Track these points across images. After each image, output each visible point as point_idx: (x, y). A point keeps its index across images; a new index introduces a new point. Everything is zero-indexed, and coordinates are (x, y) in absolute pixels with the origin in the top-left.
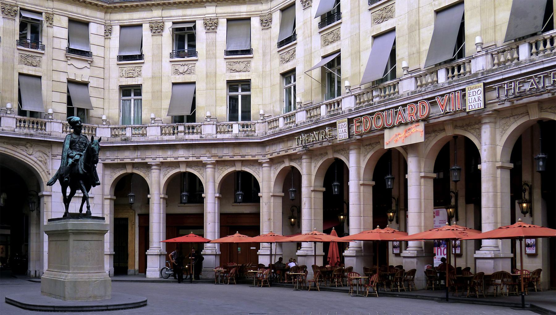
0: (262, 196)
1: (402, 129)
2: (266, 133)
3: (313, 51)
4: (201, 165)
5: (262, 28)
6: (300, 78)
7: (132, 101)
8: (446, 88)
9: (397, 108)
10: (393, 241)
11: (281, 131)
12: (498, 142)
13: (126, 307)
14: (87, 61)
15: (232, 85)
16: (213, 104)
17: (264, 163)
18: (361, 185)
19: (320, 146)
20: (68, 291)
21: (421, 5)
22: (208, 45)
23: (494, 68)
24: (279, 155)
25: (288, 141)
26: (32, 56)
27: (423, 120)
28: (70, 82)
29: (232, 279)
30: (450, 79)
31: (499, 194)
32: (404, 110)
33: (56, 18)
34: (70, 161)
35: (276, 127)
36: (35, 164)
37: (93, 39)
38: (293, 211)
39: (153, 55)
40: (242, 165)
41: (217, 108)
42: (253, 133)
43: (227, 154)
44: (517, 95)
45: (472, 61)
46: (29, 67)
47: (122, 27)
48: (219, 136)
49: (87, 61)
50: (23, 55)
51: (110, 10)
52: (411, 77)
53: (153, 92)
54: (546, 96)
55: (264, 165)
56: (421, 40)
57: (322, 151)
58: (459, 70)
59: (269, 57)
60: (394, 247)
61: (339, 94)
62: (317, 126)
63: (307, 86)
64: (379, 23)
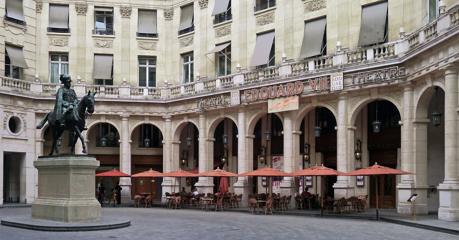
1: (282, 100)
2: (169, 97)
3: (208, 40)
4: (119, 118)
5: (165, 19)
7: (60, 64)
9: (279, 85)
10: (262, 176)
11: (182, 96)
12: (349, 113)
13: (110, 227)
14: (22, 29)
15: (142, 59)
16: (127, 73)
17: (167, 119)
20: (70, 214)
21: (295, 16)
22: (123, 27)
24: (180, 113)
25: (188, 103)
27: (297, 95)
28: (8, 45)
29: (178, 205)
30: (317, 69)
31: (349, 146)
32: (284, 87)
34: (65, 110)
35: (178, 93)
37: (26, 11)
38: (184, 154)
39: (78, 30)
40: (150, 120)
41: (131, 75)
42: (159, 96)
43: (138, 110)
47: (51, 5)
49: (22, 29)
52: (289, 65)
53: (78, 60)
54: (384, 84)
55: (166, 120)
56: (294, 40)
57: (216, 112)
58: (324, 63)
59: (171, 41)
60: (263, 181)
61: (192, 80)
62: (214, 94)
63: (203, 64)
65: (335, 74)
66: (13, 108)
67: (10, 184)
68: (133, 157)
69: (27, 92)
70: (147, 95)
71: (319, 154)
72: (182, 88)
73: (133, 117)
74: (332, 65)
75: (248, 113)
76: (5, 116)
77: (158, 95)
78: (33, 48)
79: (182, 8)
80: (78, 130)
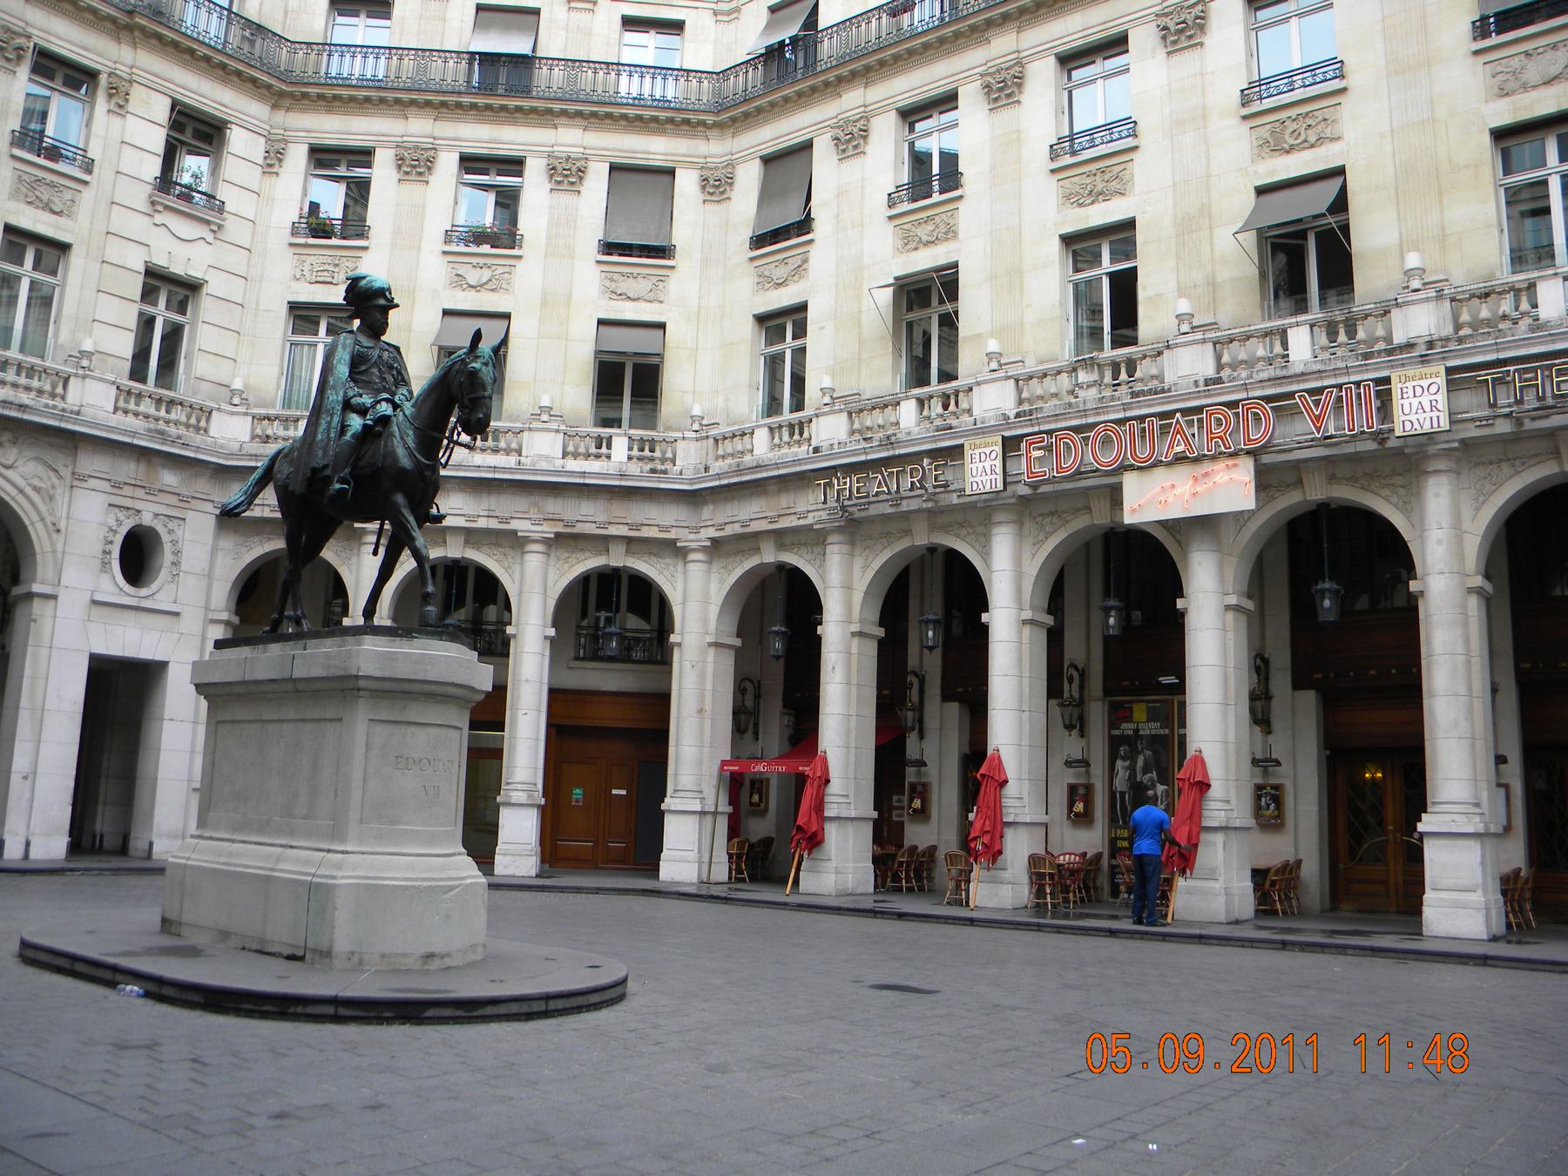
0: (679, 645)
1: (1183, 473)
4: (513, 541)
5: (702, 197)
6: (822, 328)
8: (1320, 373)
12: (1466, 526)
14: (208, 222)
17: (694, 550)
18: (1024, 622)
19: (891, 510)
23: (1462, 333)
24: (748, 530)
25: (780, 491)
26: (52, 185)
27: (1248, 453)
33: (137, 93)
34: (356, 422)
36: (20, 498)
42: (668, 466)
43: (588, 516)
44: (1550, 401)
45: (1394, 312)
46: (40, 212)
48: (573, 465)
49: (208, 222)
50: (25, 177)
51: (287, 102)
52: (1204, 341)
55: (692, 556)
61: (798, 405)
62: (891, 453)
63: (850, 348)
64: (1080, 205)
65: (1410, 373)
66: (140, 493)
67: (103, 780)
68: (556, 695)
69: (197, 439)
70: (625, 459)
71: (1309, 698)
72: (761, 436)
73: (567, 541)
74: (1388, 339)
75: (1029, 526)
76: (112, 522)
77: (663, 460)
78: (235, 289)
79: (767, 160)
80: (406, 513)
